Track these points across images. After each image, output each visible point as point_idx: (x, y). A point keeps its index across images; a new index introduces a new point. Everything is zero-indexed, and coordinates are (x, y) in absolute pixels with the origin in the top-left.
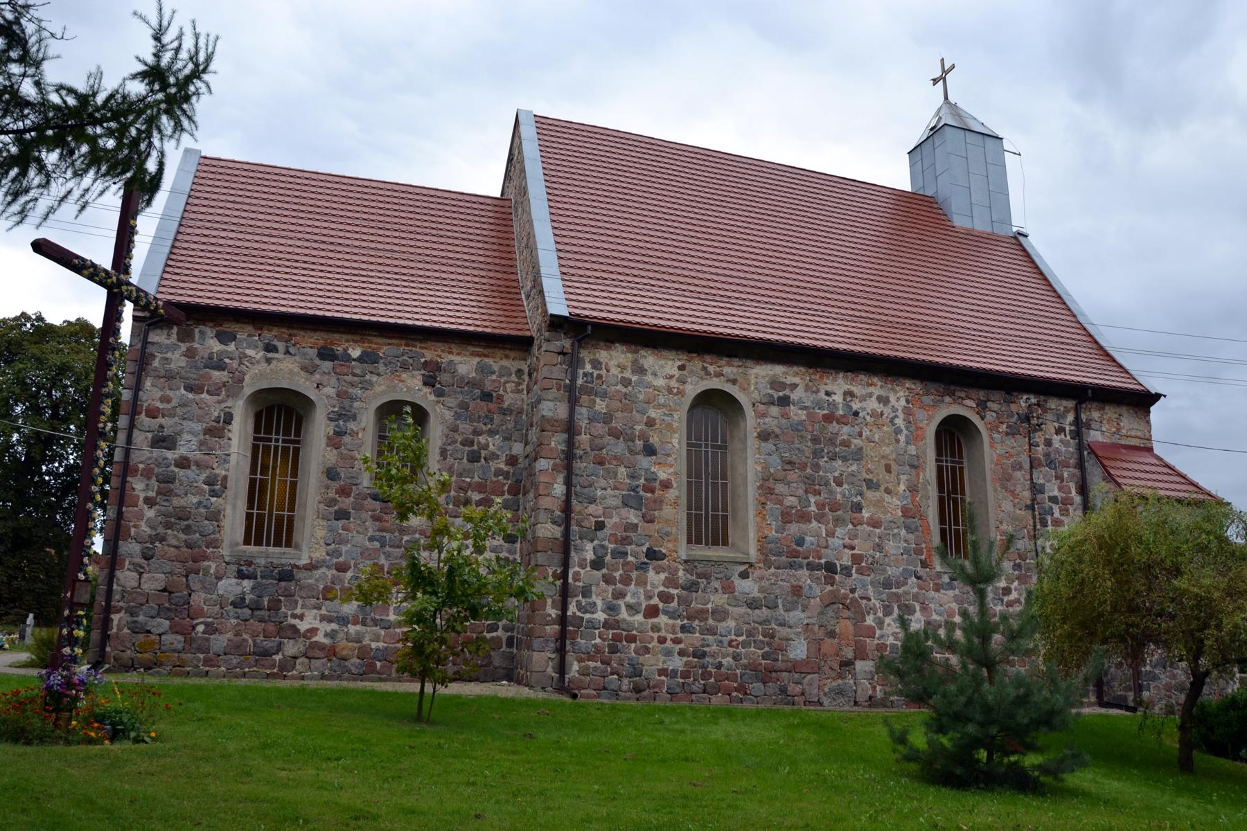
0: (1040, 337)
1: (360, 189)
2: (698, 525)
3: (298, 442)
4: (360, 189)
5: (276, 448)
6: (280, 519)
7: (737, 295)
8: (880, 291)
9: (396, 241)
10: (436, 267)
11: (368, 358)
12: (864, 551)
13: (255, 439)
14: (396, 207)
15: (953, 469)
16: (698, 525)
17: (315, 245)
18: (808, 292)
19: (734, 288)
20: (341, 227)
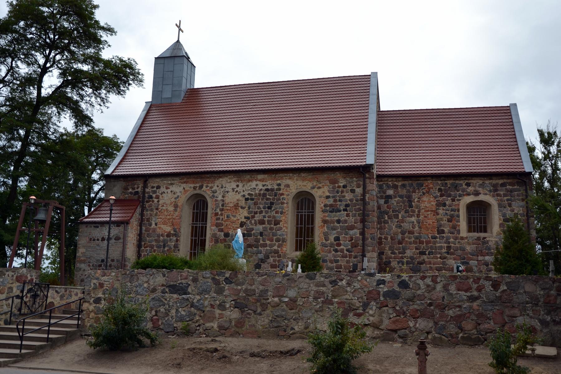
0: (335, 138)
1: (435, 114)
2: (196, 231)
3: (313, 212)
4: (435, 114)
5: (305, 215)
6: (202, 227)
7: (205, 154)
8: (281, 128)
9: (480, 137)
10: (485, 147)
11: (456, 187)
12: (462, 246)
13: (297, 212)
14: (445, 120)
15: (197, 221)
16: (196, 231)
17: (440, 148)
18: (269, 141)
19: (218, 150)
20: (502, 130)
